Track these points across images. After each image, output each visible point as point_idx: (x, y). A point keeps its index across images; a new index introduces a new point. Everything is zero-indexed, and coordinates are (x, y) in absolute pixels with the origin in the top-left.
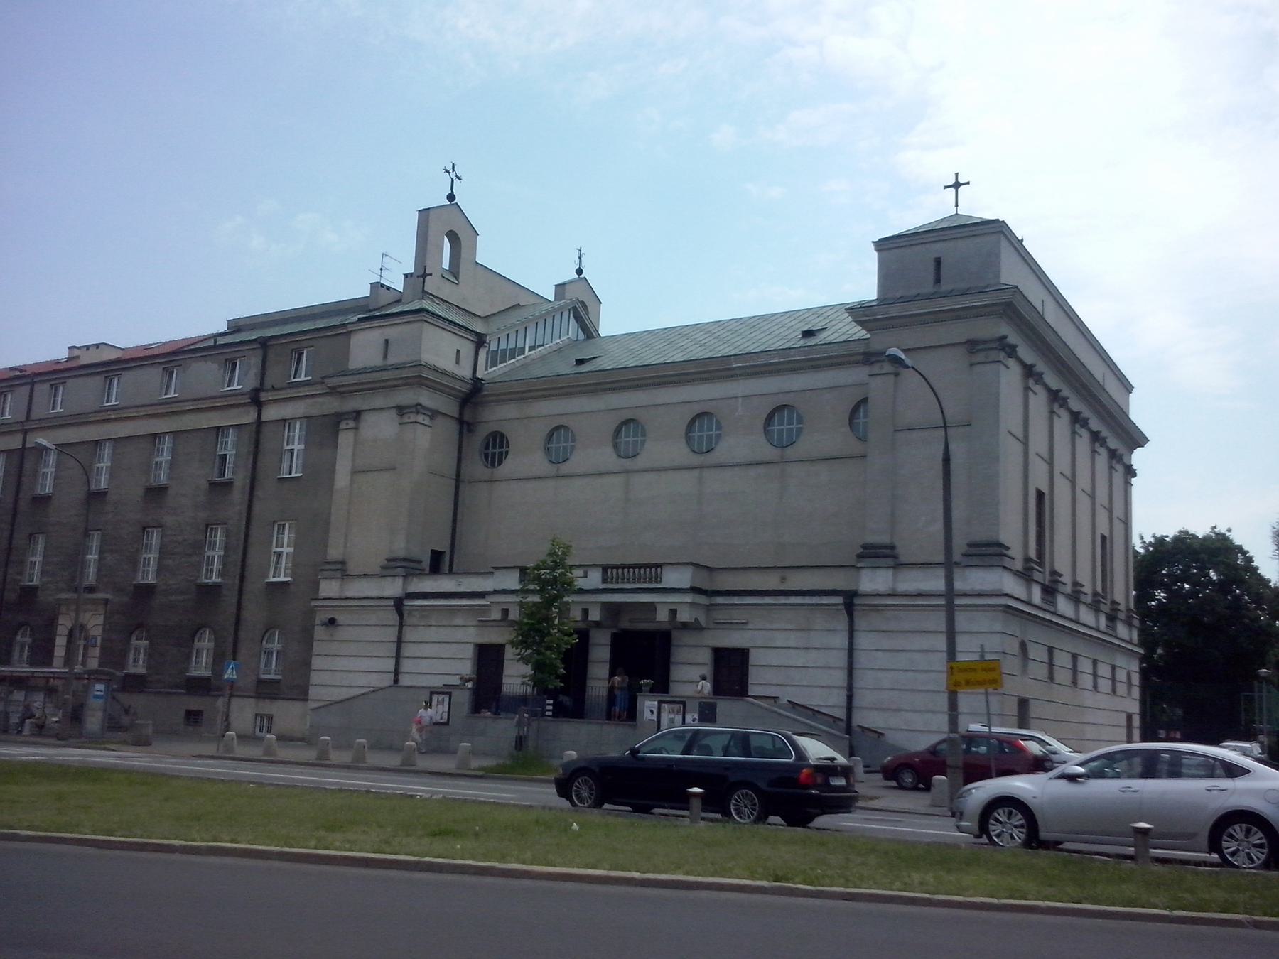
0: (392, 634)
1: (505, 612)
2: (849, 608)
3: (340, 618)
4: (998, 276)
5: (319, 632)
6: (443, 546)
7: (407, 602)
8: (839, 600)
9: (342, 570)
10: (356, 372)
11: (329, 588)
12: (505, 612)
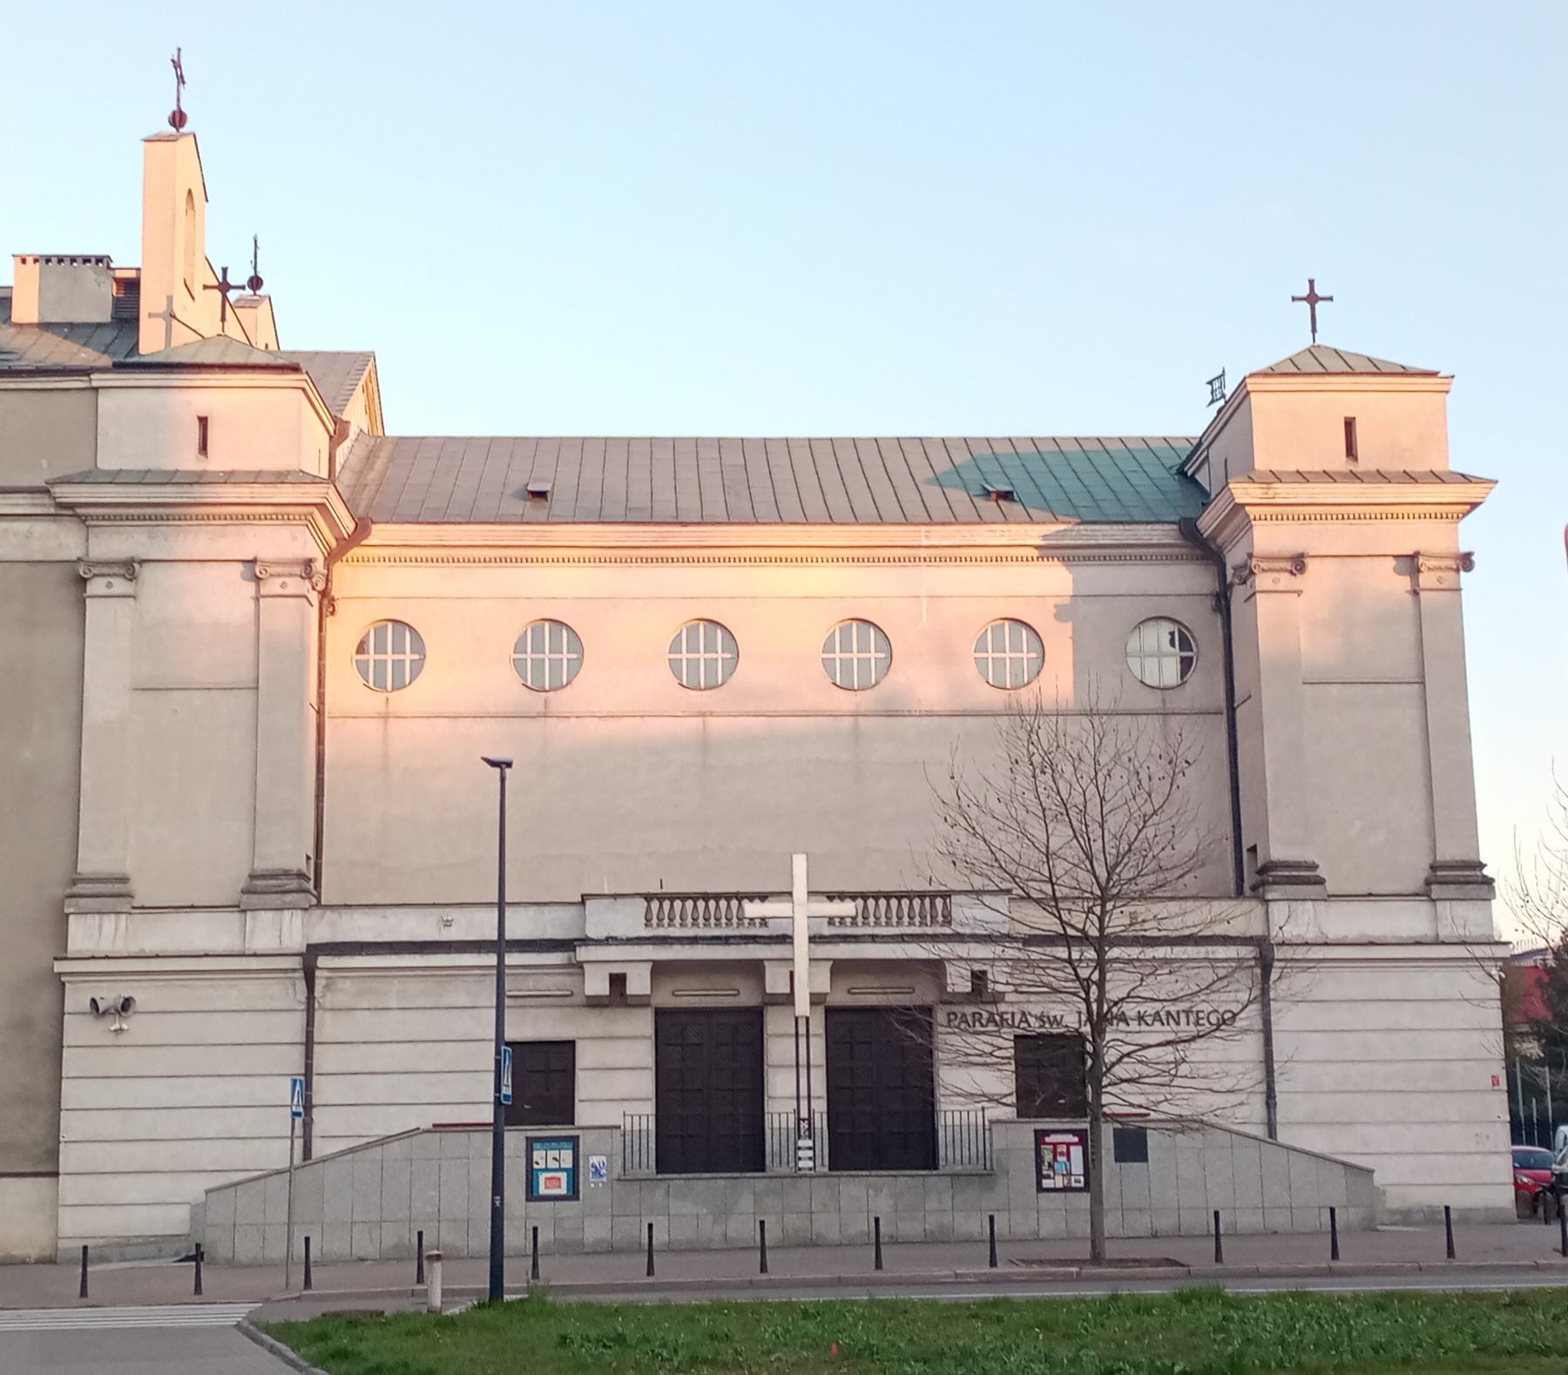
0: (293, 1026)
1: (618, 981)
2: (1265, 964)
3: (144, 996)
4: (1445, 457)
5: (77, 1030)
6: (1330, 887)
7: (323, 961)
8: (1247, 952)
9: (113, 893)
10: (115, 478)
11: (85, 934)
12: (618, 981)
